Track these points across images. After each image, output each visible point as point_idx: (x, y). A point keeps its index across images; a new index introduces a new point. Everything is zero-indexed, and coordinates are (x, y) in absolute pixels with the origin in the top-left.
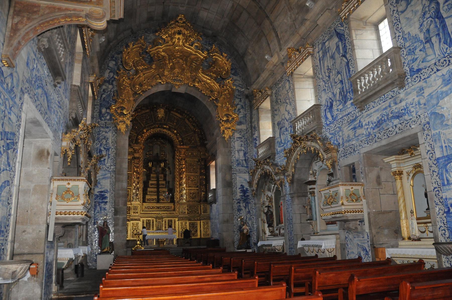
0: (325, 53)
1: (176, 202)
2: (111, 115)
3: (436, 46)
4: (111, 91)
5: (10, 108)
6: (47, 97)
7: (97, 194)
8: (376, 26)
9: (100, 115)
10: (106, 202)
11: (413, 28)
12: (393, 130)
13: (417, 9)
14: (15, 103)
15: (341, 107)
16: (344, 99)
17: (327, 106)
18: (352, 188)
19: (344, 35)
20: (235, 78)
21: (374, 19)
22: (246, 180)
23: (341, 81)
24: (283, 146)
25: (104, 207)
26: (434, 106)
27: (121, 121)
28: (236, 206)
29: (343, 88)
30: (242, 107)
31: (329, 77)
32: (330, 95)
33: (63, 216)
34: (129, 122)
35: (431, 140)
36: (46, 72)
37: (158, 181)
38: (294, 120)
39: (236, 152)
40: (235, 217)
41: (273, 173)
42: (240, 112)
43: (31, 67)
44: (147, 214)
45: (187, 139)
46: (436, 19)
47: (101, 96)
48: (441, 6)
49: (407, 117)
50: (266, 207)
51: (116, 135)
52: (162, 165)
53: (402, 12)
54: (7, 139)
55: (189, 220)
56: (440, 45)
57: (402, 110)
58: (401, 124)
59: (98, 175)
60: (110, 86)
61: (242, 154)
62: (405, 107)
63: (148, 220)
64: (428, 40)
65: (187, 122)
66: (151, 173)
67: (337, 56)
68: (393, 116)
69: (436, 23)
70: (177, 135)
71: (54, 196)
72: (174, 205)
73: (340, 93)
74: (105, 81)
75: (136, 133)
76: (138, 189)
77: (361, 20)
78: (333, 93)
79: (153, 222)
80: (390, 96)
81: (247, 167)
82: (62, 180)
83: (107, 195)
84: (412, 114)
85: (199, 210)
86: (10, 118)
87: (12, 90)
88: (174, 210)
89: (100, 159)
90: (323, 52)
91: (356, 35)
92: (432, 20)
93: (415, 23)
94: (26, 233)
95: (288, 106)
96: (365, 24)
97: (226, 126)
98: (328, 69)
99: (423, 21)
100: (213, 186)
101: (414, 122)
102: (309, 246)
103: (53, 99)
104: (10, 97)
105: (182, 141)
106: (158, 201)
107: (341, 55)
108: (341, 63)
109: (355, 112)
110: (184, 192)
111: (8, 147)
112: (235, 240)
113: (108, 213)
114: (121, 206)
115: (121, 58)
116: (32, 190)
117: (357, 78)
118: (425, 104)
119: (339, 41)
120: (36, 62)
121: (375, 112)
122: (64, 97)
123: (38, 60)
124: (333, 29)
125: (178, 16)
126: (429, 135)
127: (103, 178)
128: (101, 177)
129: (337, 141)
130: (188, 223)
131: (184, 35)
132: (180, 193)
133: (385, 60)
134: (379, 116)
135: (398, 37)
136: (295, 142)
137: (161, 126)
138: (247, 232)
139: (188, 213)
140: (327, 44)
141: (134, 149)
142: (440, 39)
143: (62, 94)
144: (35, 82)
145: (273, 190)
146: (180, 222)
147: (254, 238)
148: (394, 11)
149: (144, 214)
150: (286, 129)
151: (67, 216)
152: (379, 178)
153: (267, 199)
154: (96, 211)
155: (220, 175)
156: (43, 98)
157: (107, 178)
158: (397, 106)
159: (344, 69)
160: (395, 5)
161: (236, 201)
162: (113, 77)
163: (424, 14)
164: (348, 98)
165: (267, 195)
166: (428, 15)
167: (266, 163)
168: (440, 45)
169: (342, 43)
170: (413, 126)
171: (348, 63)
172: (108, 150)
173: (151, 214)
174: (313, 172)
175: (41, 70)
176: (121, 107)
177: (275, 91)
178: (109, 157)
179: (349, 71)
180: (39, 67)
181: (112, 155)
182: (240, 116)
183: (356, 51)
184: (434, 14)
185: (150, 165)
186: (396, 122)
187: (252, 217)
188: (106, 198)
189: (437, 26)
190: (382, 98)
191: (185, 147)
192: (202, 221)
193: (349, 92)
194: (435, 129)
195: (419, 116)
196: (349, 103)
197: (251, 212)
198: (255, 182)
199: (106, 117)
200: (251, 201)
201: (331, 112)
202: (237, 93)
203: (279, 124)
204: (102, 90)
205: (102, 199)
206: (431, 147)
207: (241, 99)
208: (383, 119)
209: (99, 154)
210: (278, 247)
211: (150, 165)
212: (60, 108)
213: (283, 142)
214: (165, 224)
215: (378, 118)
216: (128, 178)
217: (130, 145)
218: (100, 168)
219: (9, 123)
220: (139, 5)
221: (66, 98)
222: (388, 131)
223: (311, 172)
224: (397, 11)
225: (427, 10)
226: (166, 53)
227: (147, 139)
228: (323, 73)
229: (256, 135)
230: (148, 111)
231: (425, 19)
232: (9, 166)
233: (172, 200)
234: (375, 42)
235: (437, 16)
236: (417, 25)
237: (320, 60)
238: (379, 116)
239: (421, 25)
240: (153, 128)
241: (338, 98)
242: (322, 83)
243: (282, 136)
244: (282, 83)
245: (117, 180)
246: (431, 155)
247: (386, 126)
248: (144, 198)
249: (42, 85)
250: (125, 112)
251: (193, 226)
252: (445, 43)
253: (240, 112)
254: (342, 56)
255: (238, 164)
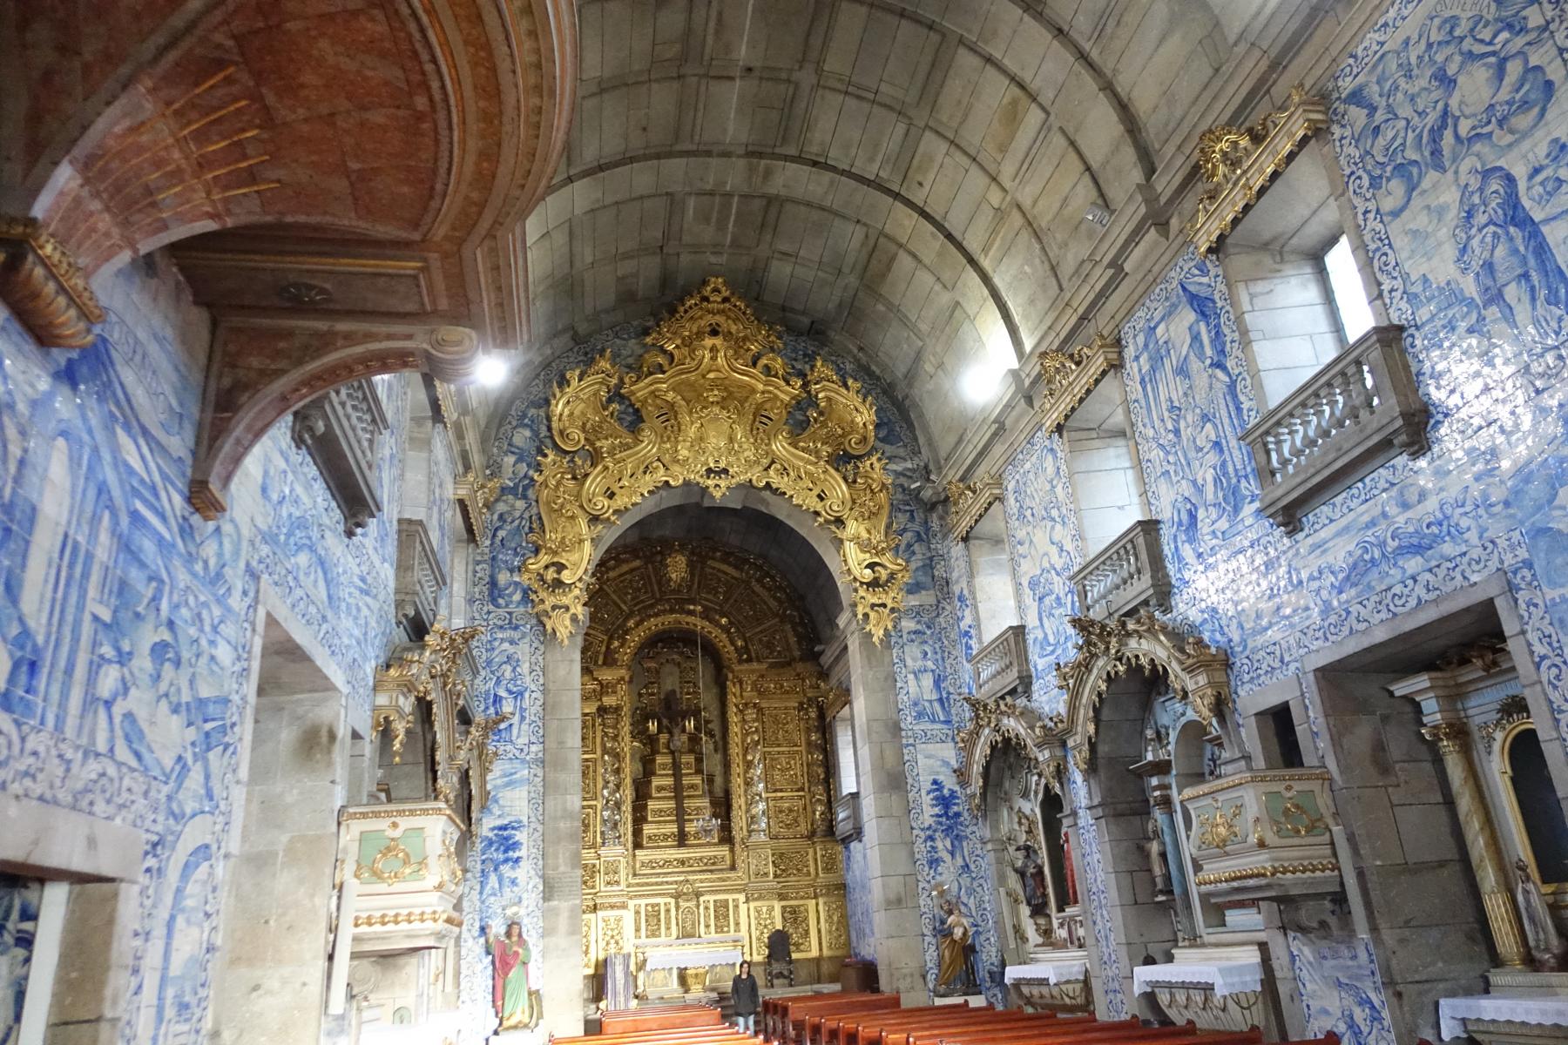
0: (1157, 361)
1: (738, 839)
2: (526, 592)
3: (1522, 312)
4: (521, 518)
5: (215, 629)
6: (325, 573)
7: (491, 835)
8: (1316, 258)
9: (491, 594)
10: (517, 860)
11: (1435, 261)
12: (1406, 591)
13: (1441, 200)
14: (229, 610)
15: (1223, 524)
16: (1232, 499)
17: (1180, 524)
18: (1289, 788)
19: (1214, 302)
20: (889, 449)
21: (1315, 231)
22: (946, 763)
23: (1217, 445)
24: (1053, 652)
25: (513, 874)
26: (1540, 508)
27: (554, 608)
28: (921, 849)
29: (1224, 464)
30: (919, 538)
31: (1177, 432)
32: (1186, 489)
33: (378, 928)
34: (580, 610)
35: (1547, 621)
36: (319, 500)
37: (677, 775)
38: (1080, 571)
39: (911, 677)
40: (921, 885)
41: (1029, 741)
42: (914, 553)
43: (275, 497)
44: (647, 884)
45: (760, 641)
46: (1512, 229)
47: (494, 536)
48: (1522, 186)
49: (1448, 548)
50: (1018, 849)
51: (542, 648)
52: (690, 725)
53: (1396, 214)
54: (206, 721)
55: (782, 897)
56: (1534, 308)
57: (1428, 526)
58: (1430, 570)
59: (489, 777)
60: (520, 504)
61: (927, 681)
62: (1440, 516)
63: (653, 906)
64: (1495, 296)
65: (758, 588)
66: (655, 752)
67: (1195, 365)
68: (1400, 547)
69: (1511, 239)
70: (728, 632)
71: (349, 868)
72: (732, 851)
73: (1217, 480)
74: (504, 490)
75: (606, 632)
76: (618, 805)
77: (1265, 246)
78: (1194, 482)
79: (668, 911)
80: (1382, 481)
81: (948, 722)
82: (376, 815)
83: (520, 836)
84: (1466, 536)
85: (811, 863)
86: (213, 658)
87: (219, 575)
88: (733, 868)
89: (494, 725)
90: (1150, 358)
91: (1252, 296)
92: (1499, 231)
93: (1440, 244)
94: (260, 992)
95: (1058, 527)
96: (1278, 258)
97: (875, 600)
98: (1172, 408)
99: (1469, 238)
100: (848, 785)
101: (1478, 562)
102: (1170, 986)
103: (345, 572)
104: (215, 595)
105: (746, 649)
106: (682, 839)
107: (1208, 362)
108: (1211, 388)
109: (1270, 538)
110: (762, 806)
111: (208, 741)
112: (929, 965)
113: (525, 896)
114: (562, 869)
115: (549, 419)
116: (281, 854)
117: (1267, 433)
118: (1507, 504)
119: (1197, 321)
120: (290, 476)
121: (1339, 534)
122: (377, 563)
123: (294, 472)
124: (1175, 283)
125: (705, 283)
126: (1536, 605)
127: (507, 785)
128: (499, 782)
129: (1223, 634)
130: (777, 906)
131: (728, 335)
132: (748, 811)
133: (1351, 370)
134: (1351, 547)
135: (1390, 292)
136: (1088, 643)
137: (679, 605)
138: (965, 933)
139: (776, 876)
140: (1160, 330)
141: (600, 683)
142: (1533, 289)
143: (371, 552)
144: (289, 535)
145: (1036, 793)
146: (752, 905)
147: (988, 956)
148: (1366, 212)
149: (638, 885)
150: (1058, 598)
151: (391, 927)
152: (1383, 749)
153: (1020, 823)
154: (488, 890)
155: (864, 751)
156: (312, 577)
157: (521, 782)
158: (1409, 514)
159: (1223, 406)
160: (1368, 196)
161: (922, 834)
162: (526, 476)
163: (1470, 215)
164: (1245, 497)
165: (1020, 810)
166: (1481, 219)
167: (1003, 707)
168: (1534, 308)
169: (1208, 324)
170: (1474, 578)
171: (1232, 387)
172: (518, 695)
173: (662, 883)
174: (1158, 733)
175: (305, 498)
176: (553, 564)
177: (1013, 482)
178: (523, 718)
179: (1239, 409)
180: (299, 490)
181: (533, 710)
182: (913, 566)
183: (1256, 346)
184: (1500, 212)
185: (653, 727)
186: (1413, 564)
187: (975, 884)
188: (516, 846)
189: (1516, 251)
190: (1354, 491)
191: (755, 665)
192: (821, 901)
193: (1246, 477)
194: (1553, 584)
195: (1492, 542)
196: (1248, 510)
197: (972, 867)
198: (977, 769)
199: (510, 596)
200: (968, 831)
201: (1191, 540)
202: (900, 497)
203: (1033, 584)
204: (496, 517)
205: (506, 851)
206: (1550, 644)
207: (912, 512)
208: (1367, 557)
209: (492, 710)
210: (1070, 987)
211: (653, 727)
212: (367, 593)
213: (1051, 640)
214: (707, 917)
215: (1350, 553)
216: (584, 775)
217: (586, 671)
218: (496, 754)
219: (212, 672)
220: (589, 259)
221: (384, 560)
222: (1389, 595)
223: (1150, 733)
224: (1378, 211)
225: (1476, 199)
226: (679, 393)
227: (642, 647)
228: (1157, 423)
229: (968, 620)
230: (637, 563)
231: (1474, 231)
232: (211, 799)
233: (727, 838)
234: (1320, 312)
235: (1513, 218)
236: (1450, 251)
237: (1142, 381)
238: (1351, 547)
239: (1464, 250)
240: (656, 615)
241: (1210, 496)
242: (1156, 454)
243: (1045, 620)
244: (1034, 459)
245: (548, 788)
246: (1554, 671)
247: (1381, 579)
248: (637, 833)
249: (310, 538)
250: (566, 576)
251: (794, 916)
252: (1552, 300)
253: (914, 553)
254: (1211, 365)
255: (920, 715)
